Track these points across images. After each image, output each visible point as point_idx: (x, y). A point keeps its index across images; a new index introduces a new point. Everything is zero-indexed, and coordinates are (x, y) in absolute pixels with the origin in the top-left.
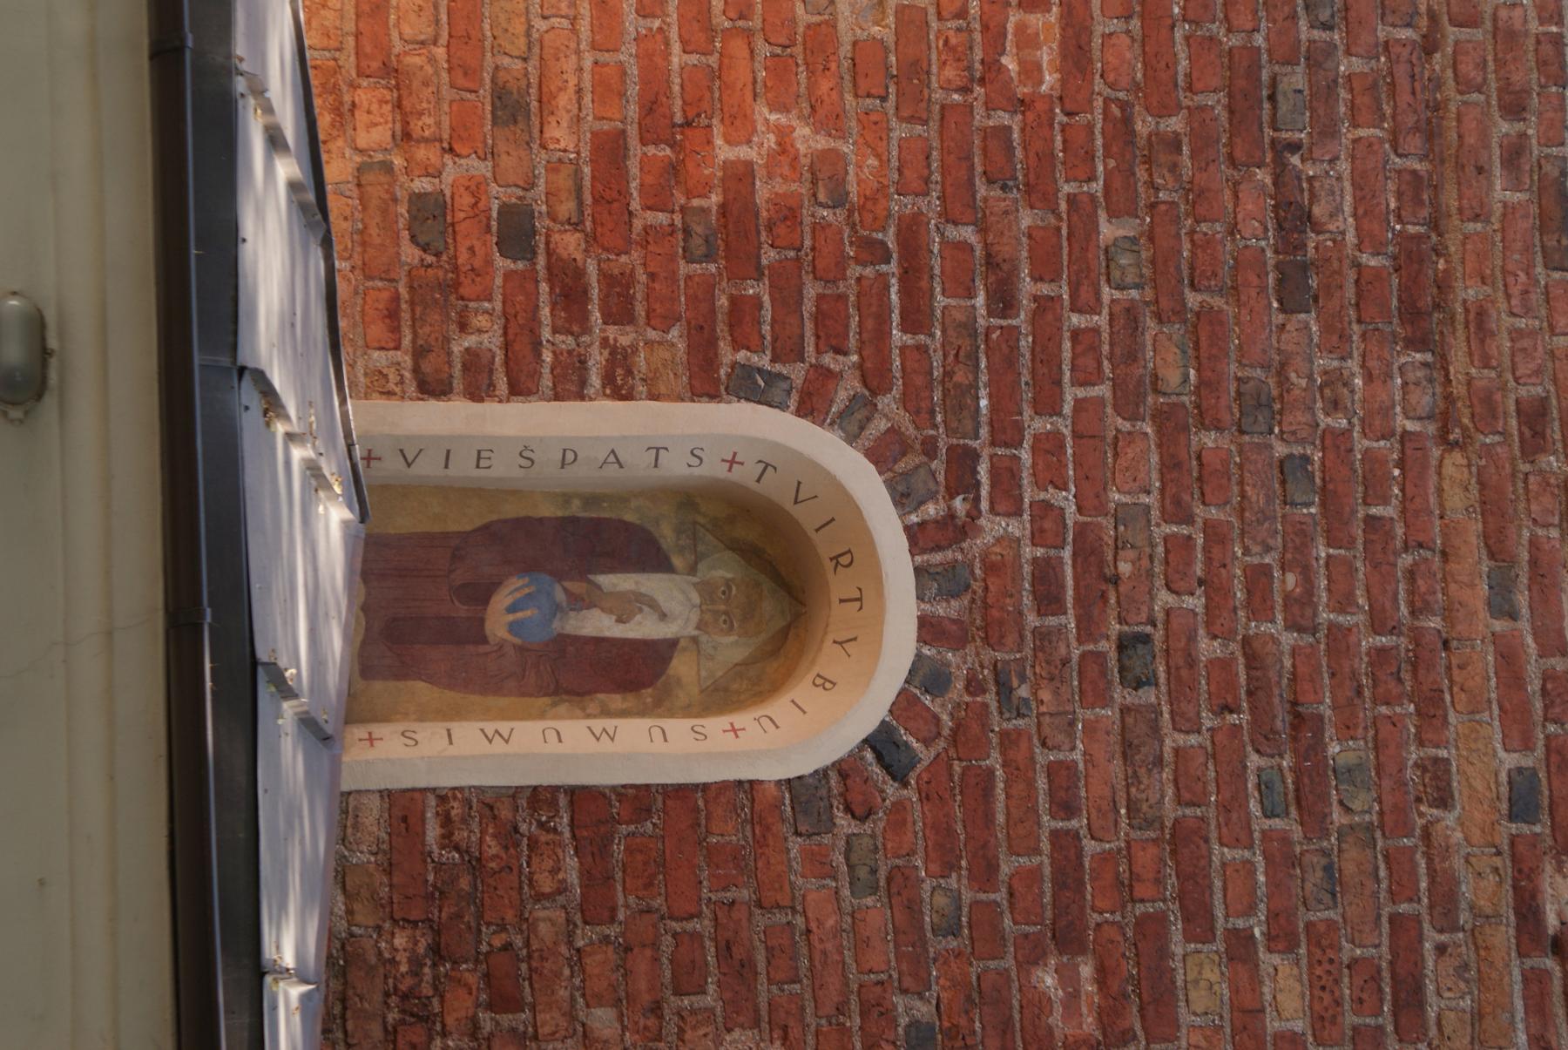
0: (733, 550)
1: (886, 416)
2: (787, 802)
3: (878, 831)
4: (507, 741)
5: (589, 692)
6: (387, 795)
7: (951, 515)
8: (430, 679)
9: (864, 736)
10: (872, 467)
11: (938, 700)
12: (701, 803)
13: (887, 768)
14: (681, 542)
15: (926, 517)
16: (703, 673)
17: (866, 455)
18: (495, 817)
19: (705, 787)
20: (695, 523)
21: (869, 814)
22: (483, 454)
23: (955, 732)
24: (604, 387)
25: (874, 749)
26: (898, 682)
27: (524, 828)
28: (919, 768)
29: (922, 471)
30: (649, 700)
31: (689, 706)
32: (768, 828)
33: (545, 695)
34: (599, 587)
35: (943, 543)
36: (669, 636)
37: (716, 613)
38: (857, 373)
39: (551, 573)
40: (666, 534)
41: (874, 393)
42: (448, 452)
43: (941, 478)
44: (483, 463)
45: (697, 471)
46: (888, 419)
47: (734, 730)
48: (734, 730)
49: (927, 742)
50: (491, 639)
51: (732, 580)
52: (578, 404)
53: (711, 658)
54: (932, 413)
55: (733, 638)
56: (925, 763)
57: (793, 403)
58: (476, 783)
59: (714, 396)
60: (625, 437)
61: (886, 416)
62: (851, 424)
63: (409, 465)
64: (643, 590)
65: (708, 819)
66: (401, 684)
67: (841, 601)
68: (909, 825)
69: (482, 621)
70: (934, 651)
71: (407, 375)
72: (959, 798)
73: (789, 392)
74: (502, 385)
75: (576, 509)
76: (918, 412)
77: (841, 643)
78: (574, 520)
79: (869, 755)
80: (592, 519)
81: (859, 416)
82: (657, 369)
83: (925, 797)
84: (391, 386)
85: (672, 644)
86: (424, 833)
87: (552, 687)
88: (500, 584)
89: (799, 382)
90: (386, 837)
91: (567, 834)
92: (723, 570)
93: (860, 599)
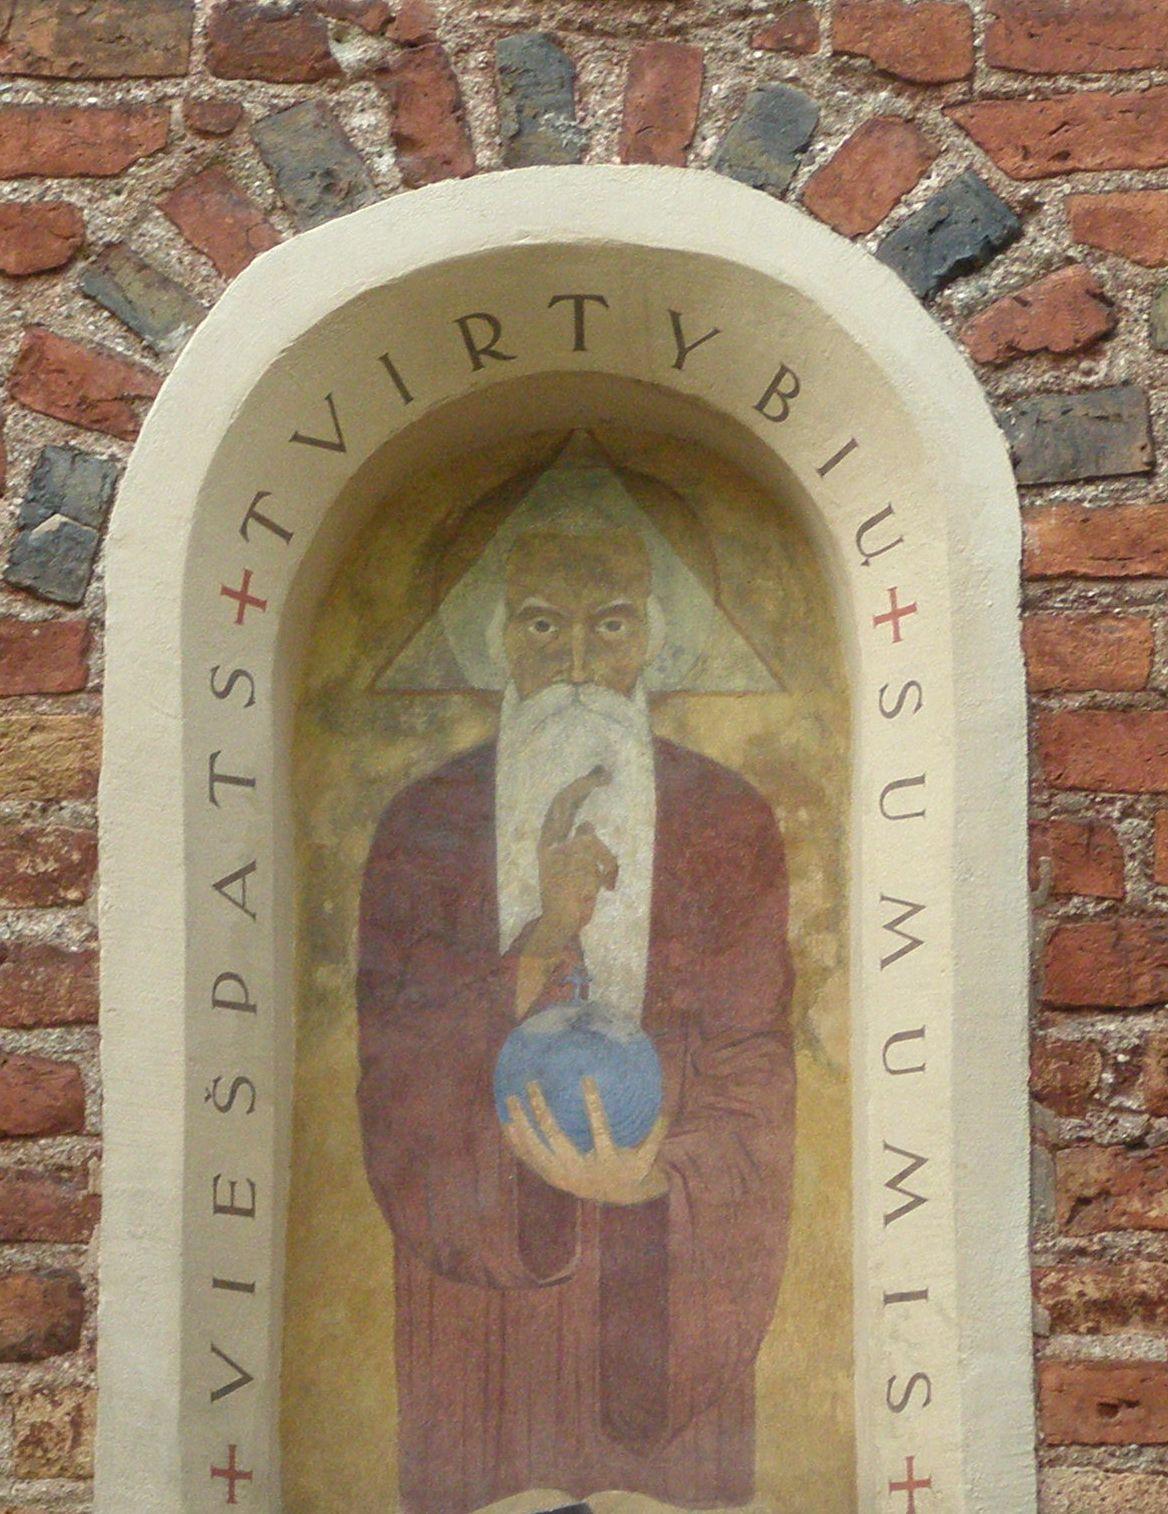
0: (436, 603)
1: (135, 222)
2: (1072, 493)
3: (1145, 277)
4: (920, 1161)
5: (785, 955)
6: (1050, 1449)
7: (377, 71)
8: (752, 1340)
9: (916, 305)
10: (260, 259)
11: (828, 120)
12: (1075, 702)
13: (993, 250)
14: (420, 724)
15: (383, 134)
16: (739, 682)
17: (233, 273)
18: (1104, 1193)
19: (1038, 690)
20: (371, 690)
21: (1102, 298)
22: (224, 1200)
23: (906, 84)
24: (62, 904)
25: (945, 281)
26: (786, 217)
27: (1129, 1127)
28: (990, 173)
29: (269, 139)
30: (803, 814)
31: (818, 718)
32: (1136, 544)
33: (790, 1063)
34: (529, 929)
35: (447, 96)
36: (648, 761)
37: (593, 647)
38: (35, 286)
39: (495, 1042)
40: (402, 760)
41: (81, 250)
42: (217, 1283)
43: (289, 93)
44: (243, 1202)
45: (264, 686)
46: (143, 216)
47: (895, 615)
48: (895, 615)
49: (927, 158)
50: (656, 1191)
51: (509, 604)
52: (105, 968)
53: (702, 660)
54: (127, 110)
55: (653, 608)
56: (979, 157)
57: (104, 448)
58: (1023, 1238)
59: (88, 636)
60: (189, 857)
61: (135, 222)
62: (156, 311)
63: (247, 1378)
64: (538, 822)
65: (1114, 687)
66: (763, 1409)
67: (580, 345)
68: (1128, 202)
69: (611, 1211)
70: (708, 127)
71: (32, 1375)
72: (1063, 82)
73: (77, 455)
74: (61, 1148)
75: (339, 978)
76: (127, 144)
77: (683, 352)
78: (367, 983)
79: (961, 293)
80: (363, 940)
81: (136, 290)
82: (22, 775)
83: (1062, 162)
84: (59, 1416)
85: (668, 756)
86: (1141, 1364)
87: (771, 1046)
88: (520, 1164)
89: (54, 430)
90: (1150, 1453)
91: (1146, 1022)
92: (484, 625)
93: (579, 301)
